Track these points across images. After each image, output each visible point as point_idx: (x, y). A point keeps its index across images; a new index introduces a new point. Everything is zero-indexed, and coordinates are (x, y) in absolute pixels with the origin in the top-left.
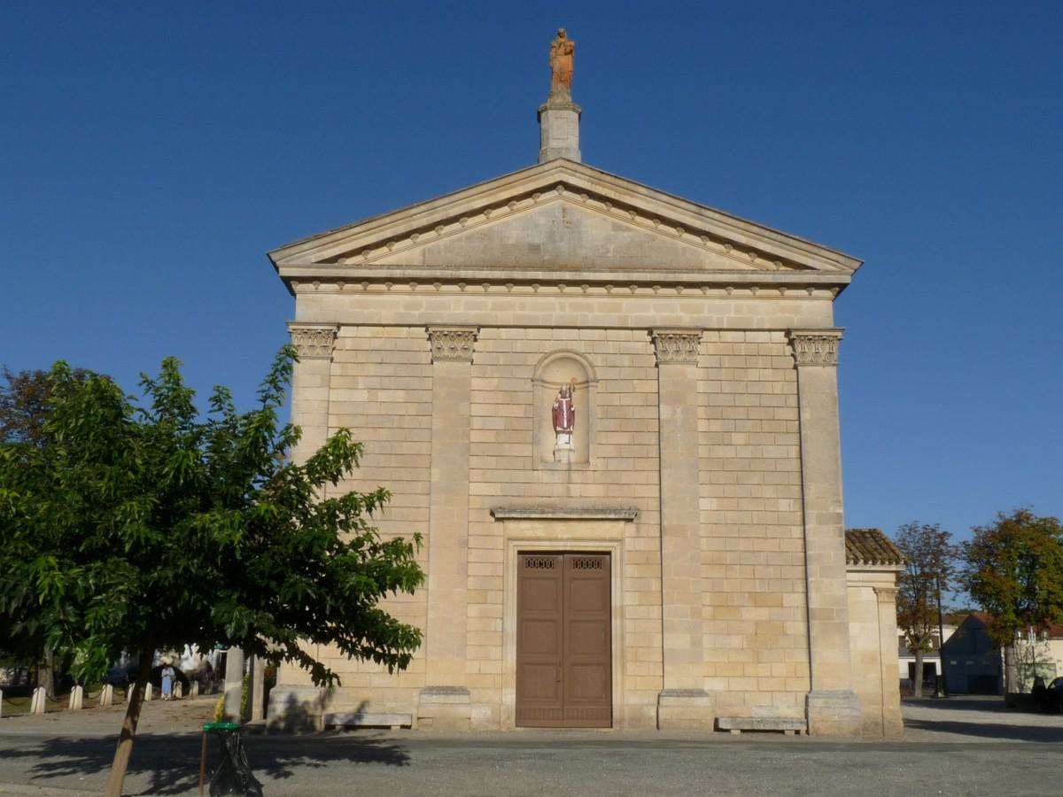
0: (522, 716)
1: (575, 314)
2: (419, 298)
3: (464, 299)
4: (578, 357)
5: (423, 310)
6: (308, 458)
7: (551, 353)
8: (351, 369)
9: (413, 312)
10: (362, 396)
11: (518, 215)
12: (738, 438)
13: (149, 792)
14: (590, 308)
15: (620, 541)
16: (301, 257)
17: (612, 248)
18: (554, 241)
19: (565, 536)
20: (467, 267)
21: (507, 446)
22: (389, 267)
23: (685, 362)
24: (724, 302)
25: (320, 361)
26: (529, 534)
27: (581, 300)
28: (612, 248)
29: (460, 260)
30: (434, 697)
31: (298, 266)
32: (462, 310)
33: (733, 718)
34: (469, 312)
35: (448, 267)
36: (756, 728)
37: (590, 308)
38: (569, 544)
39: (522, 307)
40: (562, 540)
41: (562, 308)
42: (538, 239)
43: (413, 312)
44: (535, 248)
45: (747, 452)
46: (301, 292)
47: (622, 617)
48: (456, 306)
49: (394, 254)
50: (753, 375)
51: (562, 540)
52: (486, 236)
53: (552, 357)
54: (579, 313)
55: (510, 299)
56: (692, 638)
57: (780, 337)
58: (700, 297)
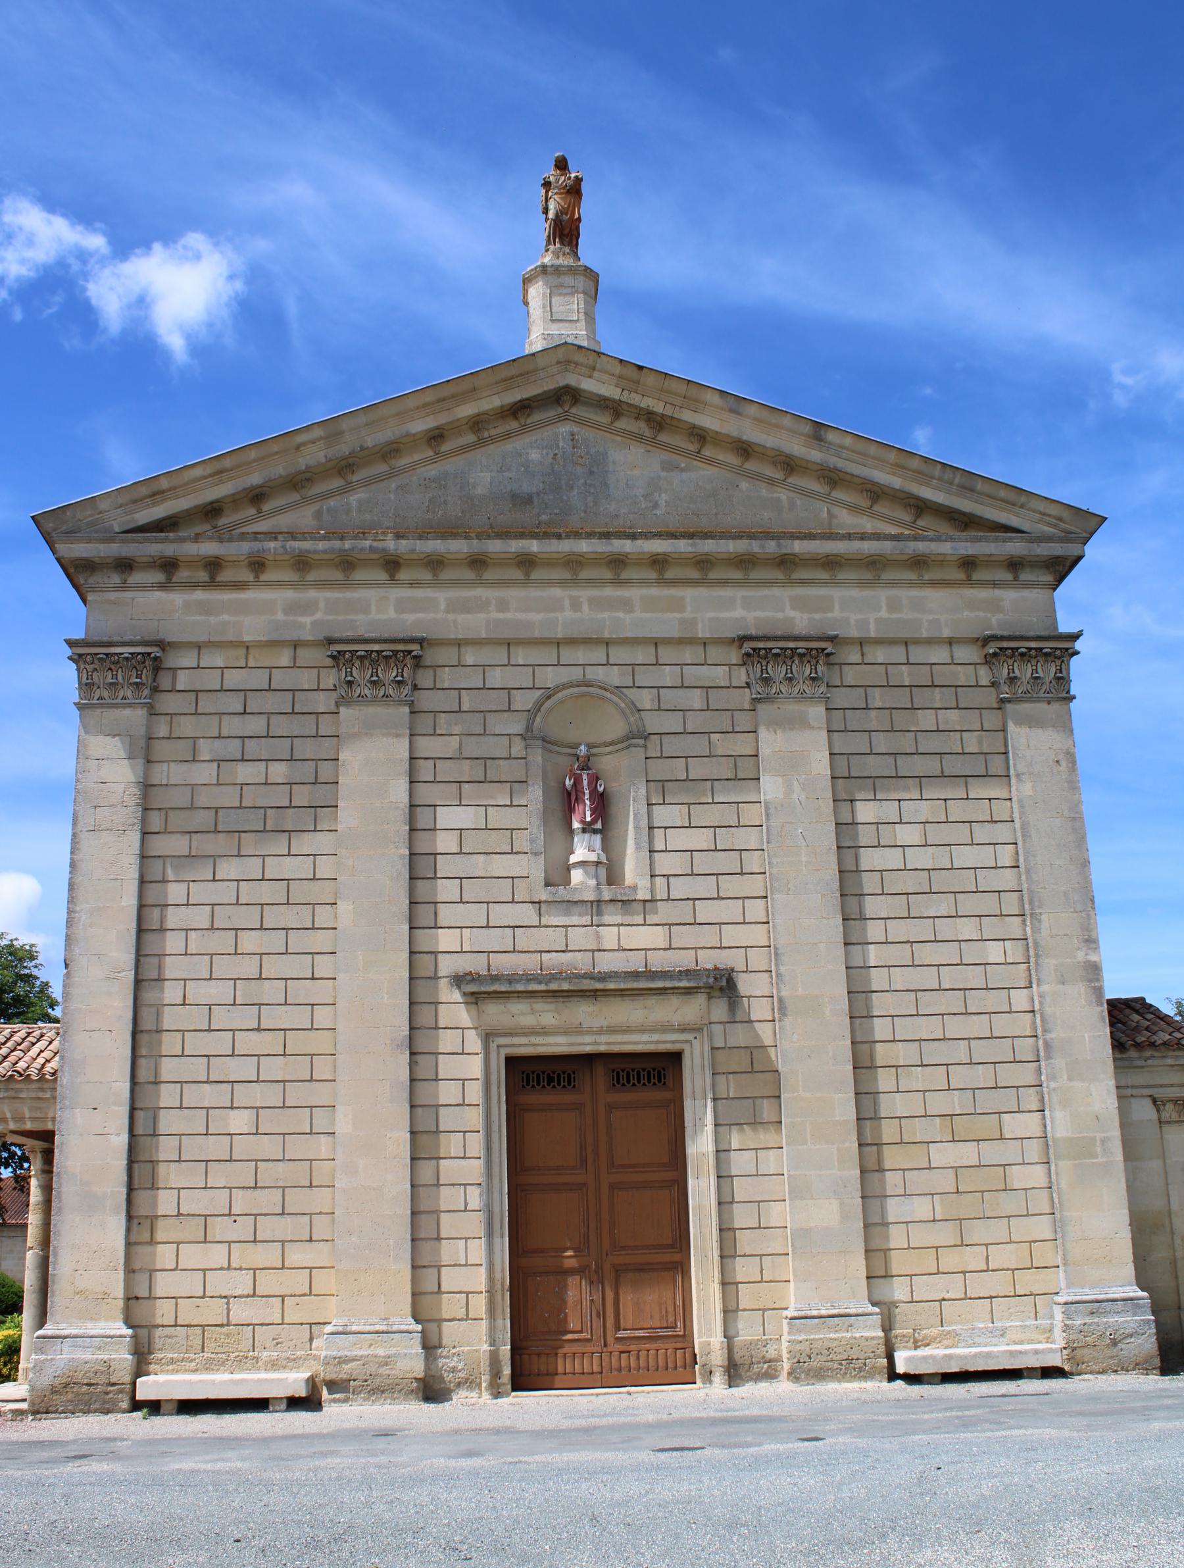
2: (312, 594)
5: (318, 616)
9: (302, 619)
14: (627, 605)
26: (528, 1021)
32: (392, 613)
41: (893, 606)
45: (922, 858)
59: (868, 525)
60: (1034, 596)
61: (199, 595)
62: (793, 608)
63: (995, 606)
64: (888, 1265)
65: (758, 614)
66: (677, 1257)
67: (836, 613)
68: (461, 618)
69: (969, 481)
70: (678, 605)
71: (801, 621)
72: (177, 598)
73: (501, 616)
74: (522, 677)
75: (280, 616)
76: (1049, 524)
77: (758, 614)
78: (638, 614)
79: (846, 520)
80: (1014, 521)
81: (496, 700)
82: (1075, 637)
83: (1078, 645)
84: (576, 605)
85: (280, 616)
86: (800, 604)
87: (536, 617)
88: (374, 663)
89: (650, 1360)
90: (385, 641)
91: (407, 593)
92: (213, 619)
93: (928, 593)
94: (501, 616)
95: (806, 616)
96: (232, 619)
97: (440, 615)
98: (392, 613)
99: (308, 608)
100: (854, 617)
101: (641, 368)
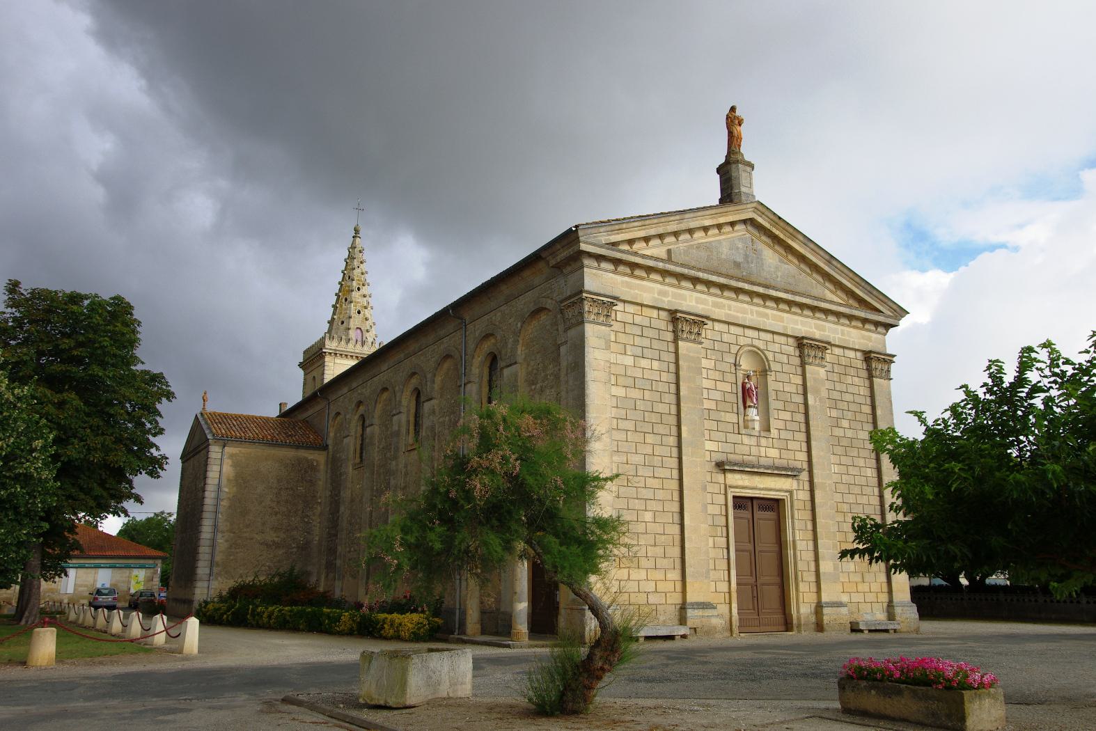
0: (744, 626)
1: (759, 319)
2: (666, 288)
3: (695, 295)
4: (759, 352)
5: (669, 299)
6: (78, 291)
7: (754, 347)
8: (622, 338)
9: (664, 299)
10: (629, 361)
11: (737, 234)
12: (845, 424)
13: (542, 710)
14: (766, 316)
15: (791, 492)
16: (595, 237)
17: (779, 274)
18: (748, 262)
19: (762, 486)
20: (704, 271)
21: (723, 414)
22: (651, 258)
23: (818, 365)
24: (835, 326)
25: (604, 327)
26: (740, 483)
27: (761, 309)
28: (779, 274)
29: (693, 263)
30: (696, 611)
31: (594, 245)
32: (694, 303)
33: (867, 623)
34: (699, 305)
35: (693, 268)
36: (877, 628)
37: (766, 316)
38: (762, 492)
39: (744, 312)
40: (760, 489)
41: (843, 334)
42: (740, 259)
43: (664, 299)
44: (737, 265)
45: (849, 433)
46: (587, 267)
47: (795, 549)
48: (691, 300)
49: (651, 248)
50: (849, 380)
51: (760, 489)
52: (708, 247)
53: (755, 349)
54: (761, 319)
55: (722, 300)
56: (834, 564)
57: (859, 355)
58: (824, 320)
59: (835, 299)
60: (879, 336)
61: (626, 279)
62: (815, 328)
63: (869, 339)
64: (786, 601)
65: (806, 329)
66: (740, 611)
67: (826, 333)
68: (717, 310)
69: (644, 229)
70: (782, 320)
71: (817, 334)
72: (619, 278)
73: (729, 312)
74: (732, 339)
75: (656, 295)
76: (891, 312)
77: (806, 329)
78: (770, 321)
79: (830, 296)
80: (881, 308)
81: (725, 348)
82: (894, 356)
83: (894, 359)
84: (752, 312)
85: (656, 295)
86: (817, 327)
87: (740, 315)
88: (690, 324)
89: (355, 727)
90: (696, 315)
91: (699, 295)
92: (632, 291)
93: (851, 330)
94: (729, 312)
95: (819, 332)
96: (639, 293)
97: (710, 308)
98: (694, 303)
99: (665, 294)
100: (832, 335)
101: (780, 218)
